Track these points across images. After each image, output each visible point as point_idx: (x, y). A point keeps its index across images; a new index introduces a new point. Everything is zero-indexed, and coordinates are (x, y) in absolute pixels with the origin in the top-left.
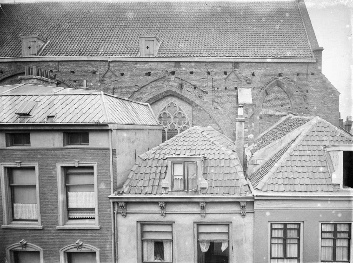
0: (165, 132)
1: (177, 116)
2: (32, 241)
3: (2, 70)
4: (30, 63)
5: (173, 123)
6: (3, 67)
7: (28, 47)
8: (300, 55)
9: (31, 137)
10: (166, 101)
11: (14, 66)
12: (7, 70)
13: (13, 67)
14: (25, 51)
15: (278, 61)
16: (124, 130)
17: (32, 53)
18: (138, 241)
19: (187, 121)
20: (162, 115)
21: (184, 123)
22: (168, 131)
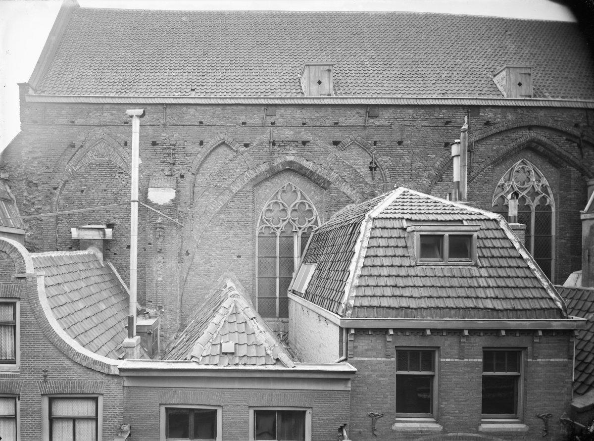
0: (276, 237)
1: (271, 207)
2: (120, 404)
3: (490, 120)
4: (539, 110)
5: (291, 221)
6: (491, 115)
7: (518, 83)
8: (428, 88)
9: (583, 224)
10: (271, 181)
11: (511, 114)
12: (499, 120)
13: (510, 116)
14: (511, 90)
15: (186, 103)
16: (12, 235)
17: (523, 94)
18: (587, 411)
19: (314, 217)
20: (271, 206)
21: (309, 221)
22: (302, 235)
